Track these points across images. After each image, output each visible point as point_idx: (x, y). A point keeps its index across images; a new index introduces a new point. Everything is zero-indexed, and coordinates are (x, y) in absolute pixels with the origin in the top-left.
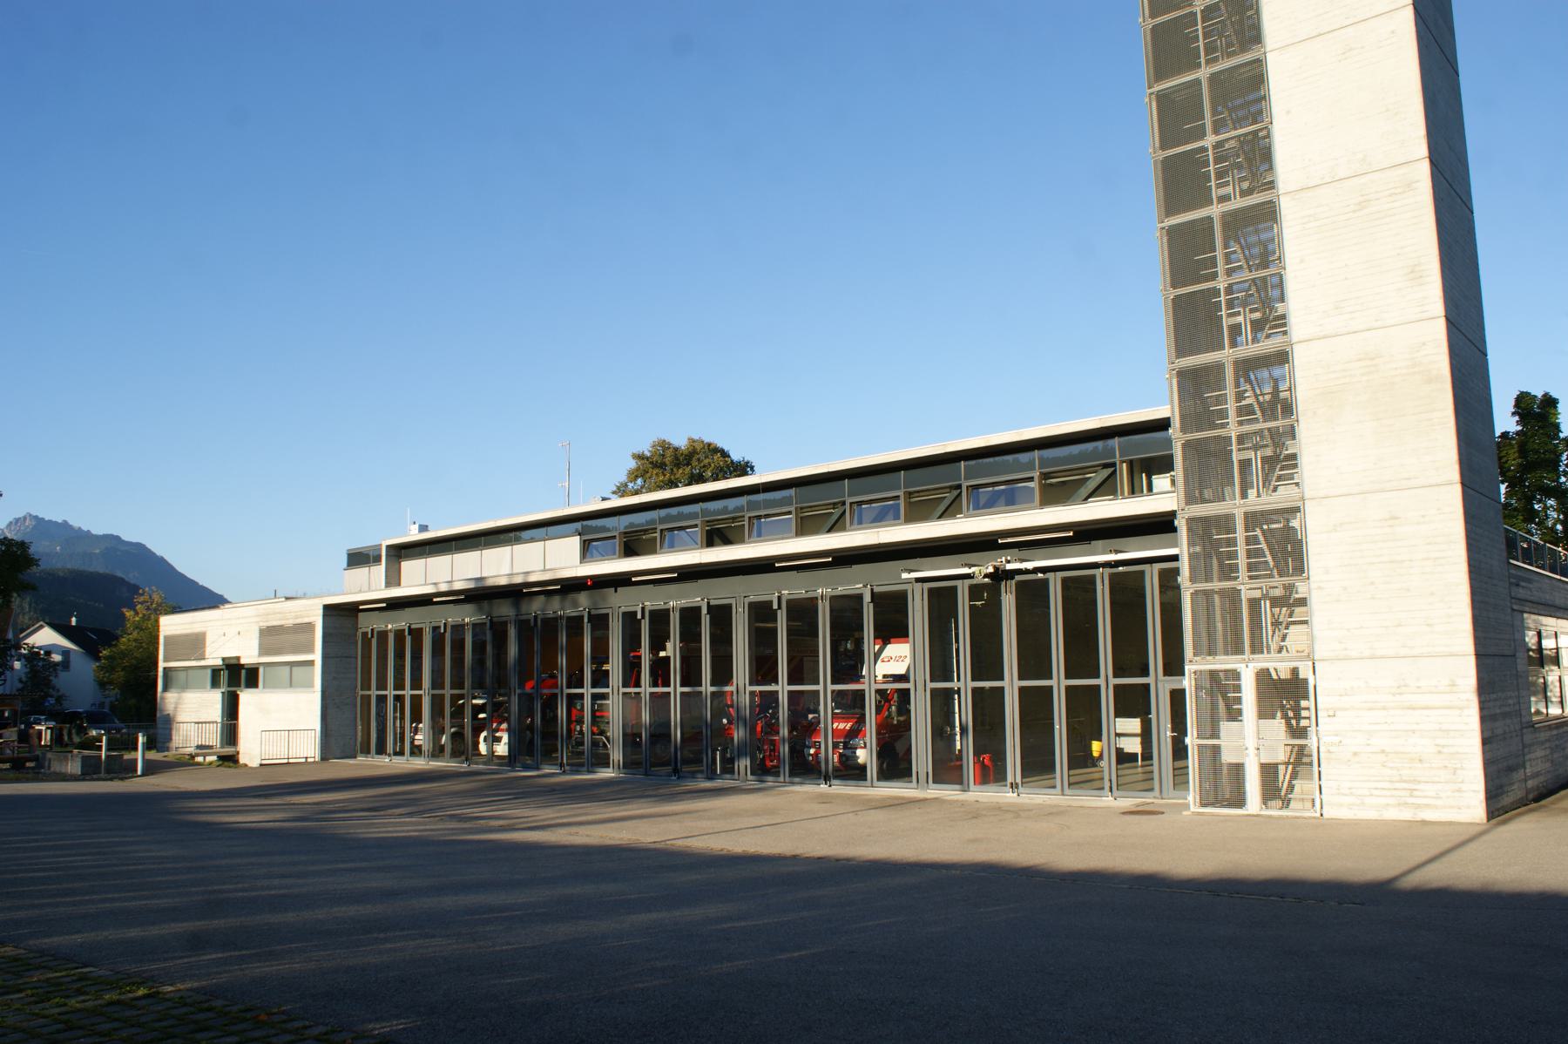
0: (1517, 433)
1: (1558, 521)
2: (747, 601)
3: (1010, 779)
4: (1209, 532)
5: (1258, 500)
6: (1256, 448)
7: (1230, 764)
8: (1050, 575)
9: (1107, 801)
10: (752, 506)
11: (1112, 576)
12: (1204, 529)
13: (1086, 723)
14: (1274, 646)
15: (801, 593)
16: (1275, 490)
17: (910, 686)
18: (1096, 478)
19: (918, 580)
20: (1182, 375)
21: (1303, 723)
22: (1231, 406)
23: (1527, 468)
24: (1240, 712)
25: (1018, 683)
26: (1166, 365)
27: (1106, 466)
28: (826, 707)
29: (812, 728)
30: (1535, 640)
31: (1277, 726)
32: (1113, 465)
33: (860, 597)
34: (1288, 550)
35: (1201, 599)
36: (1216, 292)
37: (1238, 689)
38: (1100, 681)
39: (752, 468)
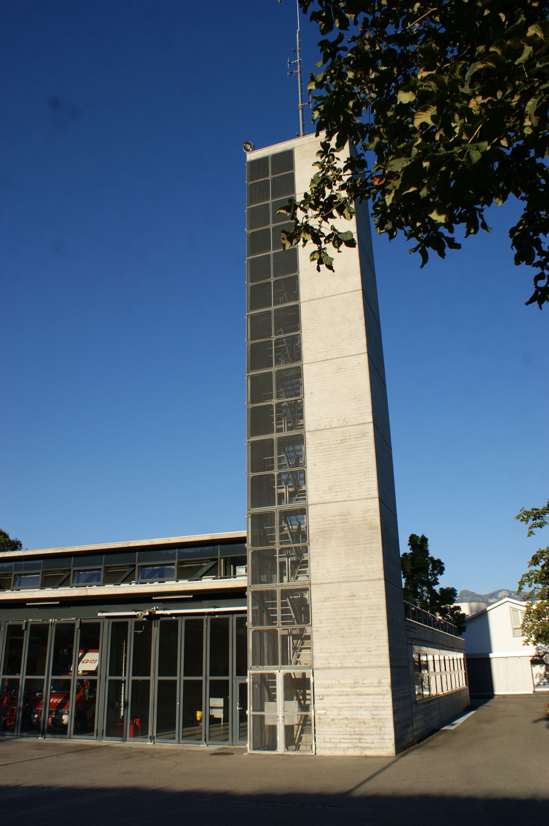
0: (410, 554)
1: (428, 597)
2: (7, 624)
3: (150, 734)
4: (263, 599)
5: (288, 583)
6: (288, 556)
7: (269, 726)
8: (179, 618)
9: (203, 747)
10: (17, 568)
11: (212, 620)
12: (259, 597)
13: (194, 700)
14: (293, 660)
15: (40, 621)
16: (297, 578)
17: (97, 678)
18: (207, 566)
19: (107, 617)
20: (254, 516)
21: (307, 702)
22: (277, 534)
23: (414, 571)
24: (275, 696)
25: (158, 678)
26: (246, 512)
27: (213, 560)
28: (47, 689)
29: (38, 701)
30: (417, 657)
31: (294, 704)
32: (217, 559)
33: (73, 625)
34: (301, 610)
35: (257, 634)
36: (273, 476)
37: (274, 683)
38: (203, 678)
39: (21, 545)
